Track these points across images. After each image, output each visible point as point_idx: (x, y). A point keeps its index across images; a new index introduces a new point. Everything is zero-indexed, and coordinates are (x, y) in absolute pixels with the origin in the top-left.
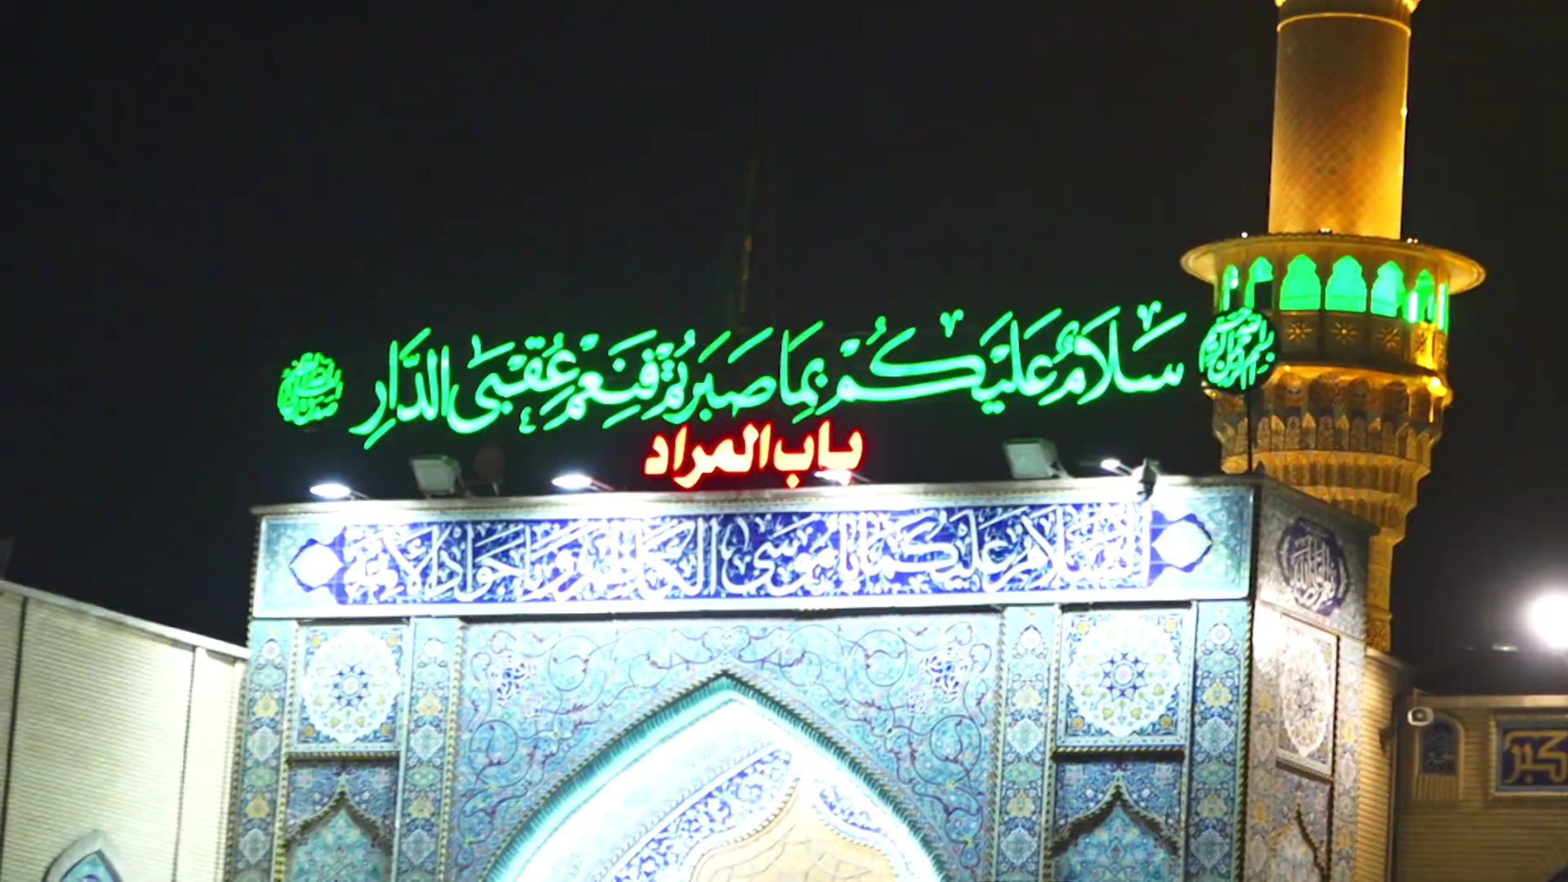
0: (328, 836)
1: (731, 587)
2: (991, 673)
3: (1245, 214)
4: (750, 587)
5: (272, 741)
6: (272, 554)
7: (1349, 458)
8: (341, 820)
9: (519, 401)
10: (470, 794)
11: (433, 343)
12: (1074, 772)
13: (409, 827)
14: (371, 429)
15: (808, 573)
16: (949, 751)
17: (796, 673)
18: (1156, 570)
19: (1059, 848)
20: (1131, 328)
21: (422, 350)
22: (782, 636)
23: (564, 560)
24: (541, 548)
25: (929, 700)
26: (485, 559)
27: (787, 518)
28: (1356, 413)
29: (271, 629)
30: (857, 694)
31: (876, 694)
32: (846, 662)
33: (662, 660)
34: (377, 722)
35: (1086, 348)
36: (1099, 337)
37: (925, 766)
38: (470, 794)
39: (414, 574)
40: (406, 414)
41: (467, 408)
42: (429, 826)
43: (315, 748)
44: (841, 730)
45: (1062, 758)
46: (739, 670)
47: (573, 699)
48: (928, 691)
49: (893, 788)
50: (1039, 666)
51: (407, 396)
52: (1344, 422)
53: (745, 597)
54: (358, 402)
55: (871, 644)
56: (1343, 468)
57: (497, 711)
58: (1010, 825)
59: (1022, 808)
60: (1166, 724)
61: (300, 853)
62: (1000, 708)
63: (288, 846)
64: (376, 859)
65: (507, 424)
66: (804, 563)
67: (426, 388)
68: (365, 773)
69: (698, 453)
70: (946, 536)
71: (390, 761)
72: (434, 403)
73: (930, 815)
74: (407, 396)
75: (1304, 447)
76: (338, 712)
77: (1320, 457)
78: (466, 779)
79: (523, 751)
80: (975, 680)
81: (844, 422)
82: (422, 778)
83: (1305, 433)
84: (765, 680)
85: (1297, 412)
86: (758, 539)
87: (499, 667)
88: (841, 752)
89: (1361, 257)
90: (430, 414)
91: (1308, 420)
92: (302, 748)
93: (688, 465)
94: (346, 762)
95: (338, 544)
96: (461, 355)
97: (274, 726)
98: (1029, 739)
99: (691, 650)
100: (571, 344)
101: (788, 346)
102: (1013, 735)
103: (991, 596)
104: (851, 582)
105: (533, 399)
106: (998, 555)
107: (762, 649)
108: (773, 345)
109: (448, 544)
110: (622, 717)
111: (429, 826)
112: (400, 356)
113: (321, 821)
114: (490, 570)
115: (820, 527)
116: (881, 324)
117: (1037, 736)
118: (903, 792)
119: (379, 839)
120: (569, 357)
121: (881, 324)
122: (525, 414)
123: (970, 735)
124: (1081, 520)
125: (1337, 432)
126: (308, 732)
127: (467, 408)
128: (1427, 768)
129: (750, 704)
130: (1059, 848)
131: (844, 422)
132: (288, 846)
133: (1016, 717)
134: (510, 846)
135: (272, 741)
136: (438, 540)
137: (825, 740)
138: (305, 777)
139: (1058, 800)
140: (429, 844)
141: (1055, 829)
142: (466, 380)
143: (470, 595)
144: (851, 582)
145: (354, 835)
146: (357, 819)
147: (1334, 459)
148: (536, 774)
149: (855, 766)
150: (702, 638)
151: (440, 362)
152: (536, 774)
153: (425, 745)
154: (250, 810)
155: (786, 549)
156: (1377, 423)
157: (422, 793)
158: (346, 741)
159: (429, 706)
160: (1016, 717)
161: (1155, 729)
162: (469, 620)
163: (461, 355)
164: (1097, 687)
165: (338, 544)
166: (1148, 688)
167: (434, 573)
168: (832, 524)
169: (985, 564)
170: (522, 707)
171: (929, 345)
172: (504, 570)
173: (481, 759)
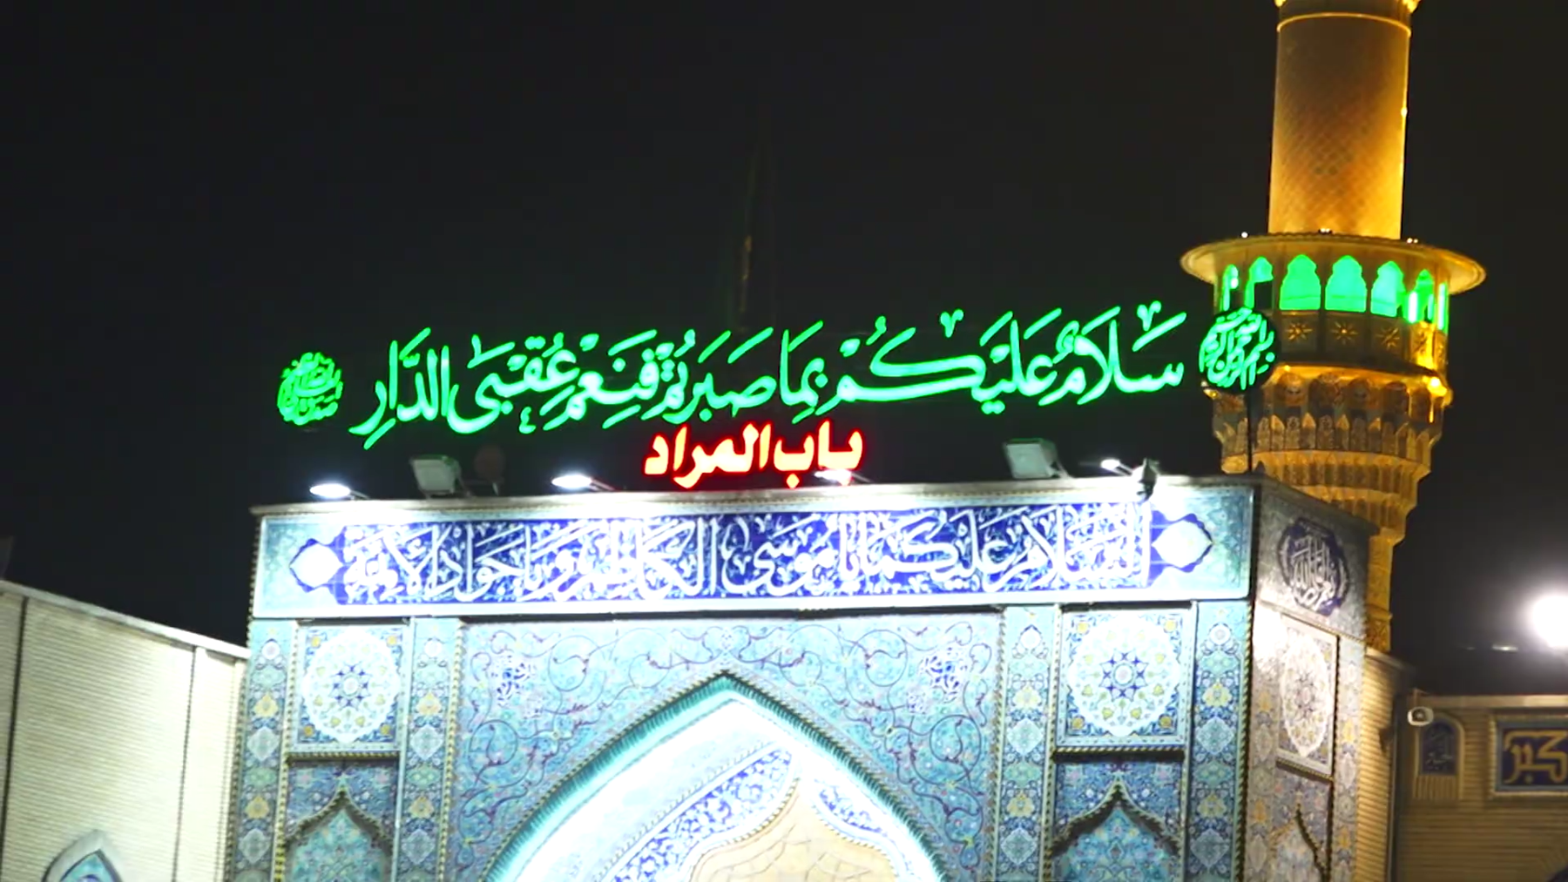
0: (328, 836)
1: (731, 587)
2: (991, 673)
4: (750, 587)
5: (272, 741)
6: (272, 554)
7: (1349, 458)
8: (341, 820)
9: (519, 401)
10: (470, 794)
11: (433, 343)
12: (1074, 772)
13: (409, 827)
14: (371, 429)
15: (808, 573)
16: (949, 751)
17: (796, 673)
18: (1156, 570)
19: (1059, 848)
20: (1131, 328)
21: (422, 350)
22: (782, 636)
23: (564, 560)
24: (541, 548)
25: (929, 700)
26: (485, 559)
27: (787, 518)
28: (1356, 413)
29: (271, 629)
30: (857, 694)
31: (876, 694)
32: (846, 662)
33: (662, 660)
34: (377, 722)
35: (1086, 348)
36: (1099, 337)
37: (925, 766)
38: (470, 794)
39: (414, 574)
40: (406, 414)
41: (467, 408)
42: (429, 826)
43: (315, 748)
44: (841, 730)
45: (1062, 758)
46: (739, 670)
47: (573, 699)
48: (928, 691)
49: (893, 788)
50: (1039, 666)
51: (407, 396)
52: (1344, 422)
53: (745, 597)
54: (358, 402)
55: (871, 644)
56: (1343, 468)
57: (497, 711)
58: (1010, 825)
59: (1022, 808)
60: (1166, 724)
61: (300, 853)
62: (1000, 708)
63: (288, 846)
64: (376, 859)
65: (507, 424)
66: (804, 563)
67: (426, 388)
68: (365, 773)
69: (698, 453)
70: (946, 536)
71: (390, 761)
72: (434, 403)
73: (930, 815)
74: (407, 396)
75: (1304, 447)
76: (338, 712)
77: (1320, 457)
78: (466, 779)
79: (523, 751)
80: (975, 680)
81: (844, 422)
82: (422, 778)
83: (1305, 433)
84: (765, 680)
85: (1297, 412)
86: (758, 539)
87: (499, 667)
88: (841, 752)
90: (430, 414)
91: (1308, 420)
92: (302, 748)
93: (688, 465)
94: (346, 762)
95: (338, 544)
96: (461, 355)
97: (274, 726)
98: (1029, 739)
99: (691, 650)
100: (571, 344)
101: (788, 346)
102: (1013, 735)
103: (991, 596)
104: (851, 582)
105: (533, 399)
106: (998, 555)
107: (762, 649)
108: (773, 345)
109: (448, 544)
110: (622, 717)
111: (429, 826)
112: (400, 356)
113: (321, 821)
114: (490, 570)
115: (820, 527)
116: (881, 324)
117: (1037, 736)
118: (903, 792)
119: (379, 839)
120: (569, 357)
121: (881, 324)
122: (525, 414)
123: (970, 735)
124: (1081, 520)
125: (1337, 432)
126: (308, 732)
127: (467, 408)
128: (1427, 768)
129: (750, 704)
130: (1059, 848)
131: (844, 422)
132: (288, 846)
133: (1016, 717)
134: (510, 846)
135: (272, 741)
136: (438, 540)
137: (825, 740)
138: (305, 777)
139: (1058, 800)
140: (429, 844)
141: (1055, 829)
142: (466, 380)
143: (470, 595)
144: (851, 582)
145: (354, 835)
146: (357, 819)
147: (1334, 459)
148: (536, 774)
149: (855, 766)
150: (702, 638)
151: (440, 362)
152: (536, 774)
153: (425, 745)
154: (250, 810)
155: (786, 549)
156: (1377, 423)
157: (422, 793)
158: (346, 741)
159: (429, 706)
160: (1016, 717)
161: (1155, 729)
162: (469, 620)
163: (461, 355)
164: (1097, 687)
165: (338, 544)
166: (1148, 688)
167: (434, 573)
168: (832, 524)
169: (985, 564)
170: (522, 707)
171: (929, 345)
172: (504, 570)
173: (481, 759)
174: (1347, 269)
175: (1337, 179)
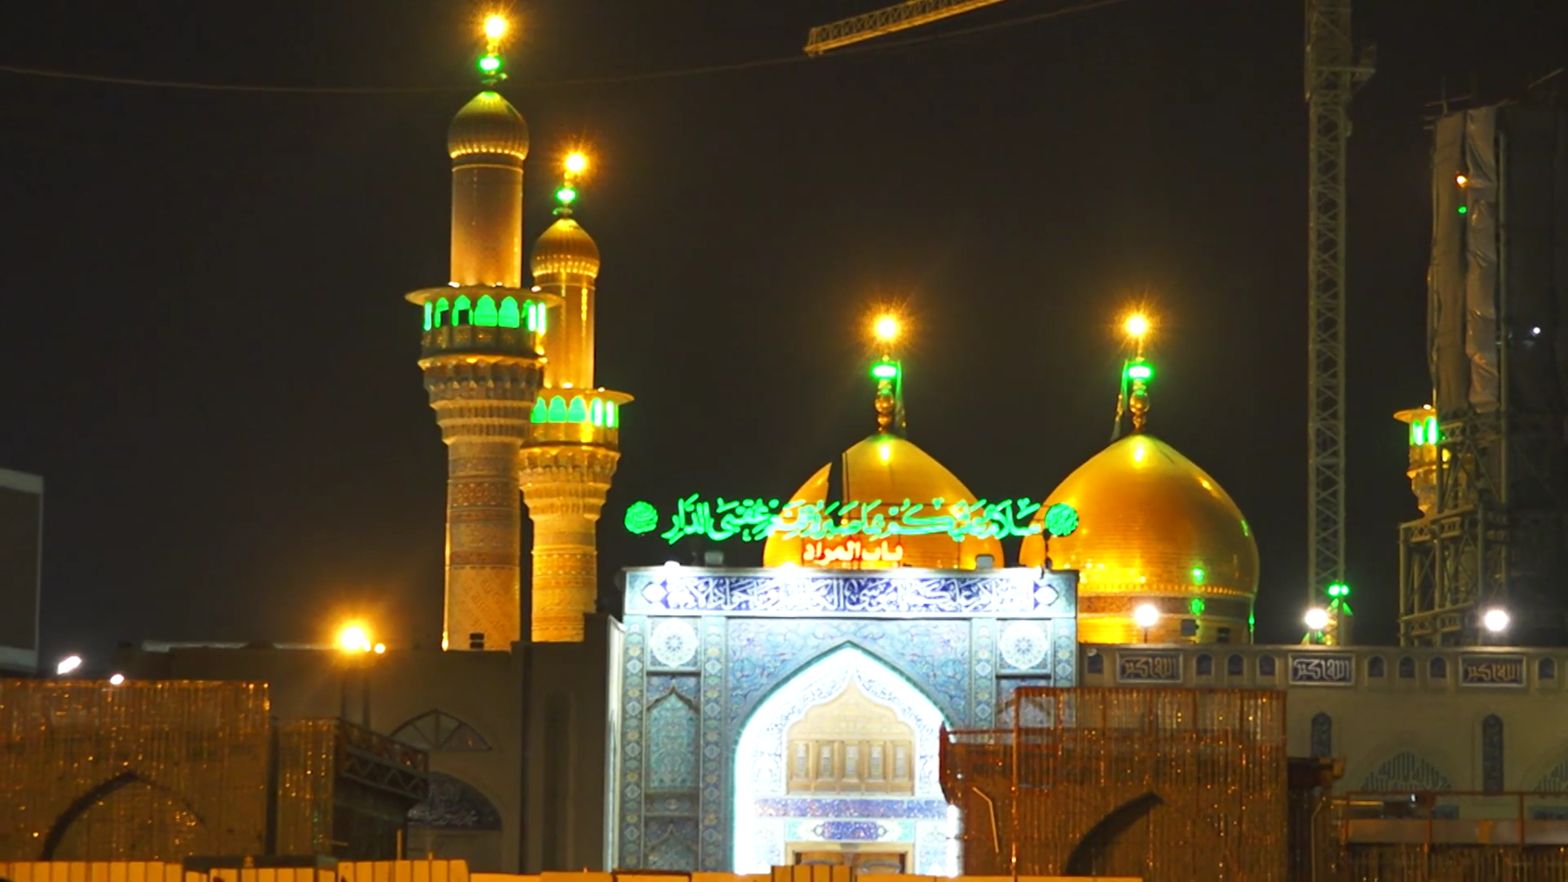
0: (667, 704)
1: (849, 606)
2: (967, 644)
3: (438, 276)
4: (858, 607)
5: (639, 666)
6: (632, 587)
7: (508, 403)
8: (673, 698)
9: (744, 527)
10: (735, 689)
11: (701, 500)
12: (1004, 683)
13: (708, 702)
14: (672, 536)
15: (882, 603)
16: (950, 673)
17: (880, 642)
18: (1036, 604)
19: (999, 712)
20: (1016, 509)
21: (695, 503)
22: (873, 628)
23: (773, 594)
24: (762, 588)
25: (940, 653)
26: (736, 593)
27: (874, 580)
28: (514, 380)
29: (634, 619)
30: (908, 651)
31: (917, 651)
32: (903, 638)
33: (820, 635)
34: (688, 658)
35: (998, 516)
36: (1003, 511)
37: (941, 679)
38: (735, 689)
39: (702, 598)
40: (689, 530)
41: (718, 527)
42: (716, 701)
43: (659, 669)
44: (901, 664)
45: (999, 677)
46: (856, 640)
47: (780, 651)
48: (940, 651)
49: (927, 688)
50: (988, 641)
51: (689, 521)
52: (508, 385)
53: (855, 611)
54: (665, 523)
55: (913, 631)
56: (491, 408)
57: (744, 655)
58: (979, 703)
59: (984, 696)
60: (1043, 665)
61: (655, 712)
62: (970, 658)
63: (649, 709)
64: (691, 714)
65: (738, 536)
66: (881, 598)
67: (694, 518)
68: (684, 680)
69: (827, 552)
70: (945, 589)
71: (697, 675)
72: (702, 523)
73: (942, 698)
74: (689, 521)
75: (488, 397)
76: (669, 654)
77: (495, 403)
78: (732, 682)
79: (758, 671)
80: (960, 646)
81: (895, 541)
82: (713, 681)
83: (488, 389)
84: (867, 645)
85: (484, 379)
86: (861, 588)
87: (744, 637)
88: (901, 673)
89: (468, 296)
90: (701, 531)
91: (491, 384)
92: (652, 669)
93: (822, 557)
94: (674, 675)
95: (664, 584)
96: (713, 507)
97: (640, 659)
98: (984, 670)
99: (833, 631)
100: (766, 503)
101: (865, 509)
102: (978, 668)
103: (966, 613)
104: (904, 607)
105: (750, 527)
106: (968, 597)
107: (865, 632)
108: (859, 509)
109: (717, 586)
110: (803, 659)
111: (716, 701)
112: (683, 506)
113: (664, 698)
114: (738, 597)
115: (888, 584)
116: (907, 502)
117: (988, 669)
118: (930, 689)
119: (693, 706)
120: (765, 509)
121: (907, 502)
122: (746, 532)
123: (959, 668)
124: (1003, 585)
125: (505, 391)
126: (655, 662)
127: (718, 527)
128: (1091, 671)
129: (859, 653)
130: (999, 712)
131: (895, 541)
132: (649, 709)
133: (979, 661)
134: (754, 708)
135: (639, 666)
136: (712, 583)
137: (894, 668)
138: (655, 681)
139: (999, 693)
140: (717, 708)
141: (998, 704)
142: (717, 518)
143: (729, 607)
144: (904, 607)
145: (680, 704)
146: (681, 698)
147: (502, 403)
148: (764, 680)
149: (909, 679)
150: (837, 628)
151: (704, 508)
152: (764, 680)
153: (712, 668)
154: (630, 693)
155: (874, 593)
156: (523, 385)
157: (713, 687)
158: (673, 665)
159: (713, 652)
160: (979, 661)
161: (1038, 667)
162: (729, 617)
163: (713, 507)
164: (1013, 650)
165: (664, 584)
166: (1034, 651)
167: (712, 598)
168: (894, 584)
169: (961, 600)
170: (758, 653)
171: (928, 511)
172: (744, 597)
173: (739, 674)
174: (486, 301)
175: (492, 253)
